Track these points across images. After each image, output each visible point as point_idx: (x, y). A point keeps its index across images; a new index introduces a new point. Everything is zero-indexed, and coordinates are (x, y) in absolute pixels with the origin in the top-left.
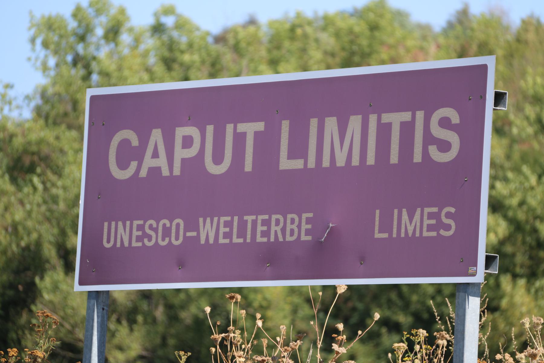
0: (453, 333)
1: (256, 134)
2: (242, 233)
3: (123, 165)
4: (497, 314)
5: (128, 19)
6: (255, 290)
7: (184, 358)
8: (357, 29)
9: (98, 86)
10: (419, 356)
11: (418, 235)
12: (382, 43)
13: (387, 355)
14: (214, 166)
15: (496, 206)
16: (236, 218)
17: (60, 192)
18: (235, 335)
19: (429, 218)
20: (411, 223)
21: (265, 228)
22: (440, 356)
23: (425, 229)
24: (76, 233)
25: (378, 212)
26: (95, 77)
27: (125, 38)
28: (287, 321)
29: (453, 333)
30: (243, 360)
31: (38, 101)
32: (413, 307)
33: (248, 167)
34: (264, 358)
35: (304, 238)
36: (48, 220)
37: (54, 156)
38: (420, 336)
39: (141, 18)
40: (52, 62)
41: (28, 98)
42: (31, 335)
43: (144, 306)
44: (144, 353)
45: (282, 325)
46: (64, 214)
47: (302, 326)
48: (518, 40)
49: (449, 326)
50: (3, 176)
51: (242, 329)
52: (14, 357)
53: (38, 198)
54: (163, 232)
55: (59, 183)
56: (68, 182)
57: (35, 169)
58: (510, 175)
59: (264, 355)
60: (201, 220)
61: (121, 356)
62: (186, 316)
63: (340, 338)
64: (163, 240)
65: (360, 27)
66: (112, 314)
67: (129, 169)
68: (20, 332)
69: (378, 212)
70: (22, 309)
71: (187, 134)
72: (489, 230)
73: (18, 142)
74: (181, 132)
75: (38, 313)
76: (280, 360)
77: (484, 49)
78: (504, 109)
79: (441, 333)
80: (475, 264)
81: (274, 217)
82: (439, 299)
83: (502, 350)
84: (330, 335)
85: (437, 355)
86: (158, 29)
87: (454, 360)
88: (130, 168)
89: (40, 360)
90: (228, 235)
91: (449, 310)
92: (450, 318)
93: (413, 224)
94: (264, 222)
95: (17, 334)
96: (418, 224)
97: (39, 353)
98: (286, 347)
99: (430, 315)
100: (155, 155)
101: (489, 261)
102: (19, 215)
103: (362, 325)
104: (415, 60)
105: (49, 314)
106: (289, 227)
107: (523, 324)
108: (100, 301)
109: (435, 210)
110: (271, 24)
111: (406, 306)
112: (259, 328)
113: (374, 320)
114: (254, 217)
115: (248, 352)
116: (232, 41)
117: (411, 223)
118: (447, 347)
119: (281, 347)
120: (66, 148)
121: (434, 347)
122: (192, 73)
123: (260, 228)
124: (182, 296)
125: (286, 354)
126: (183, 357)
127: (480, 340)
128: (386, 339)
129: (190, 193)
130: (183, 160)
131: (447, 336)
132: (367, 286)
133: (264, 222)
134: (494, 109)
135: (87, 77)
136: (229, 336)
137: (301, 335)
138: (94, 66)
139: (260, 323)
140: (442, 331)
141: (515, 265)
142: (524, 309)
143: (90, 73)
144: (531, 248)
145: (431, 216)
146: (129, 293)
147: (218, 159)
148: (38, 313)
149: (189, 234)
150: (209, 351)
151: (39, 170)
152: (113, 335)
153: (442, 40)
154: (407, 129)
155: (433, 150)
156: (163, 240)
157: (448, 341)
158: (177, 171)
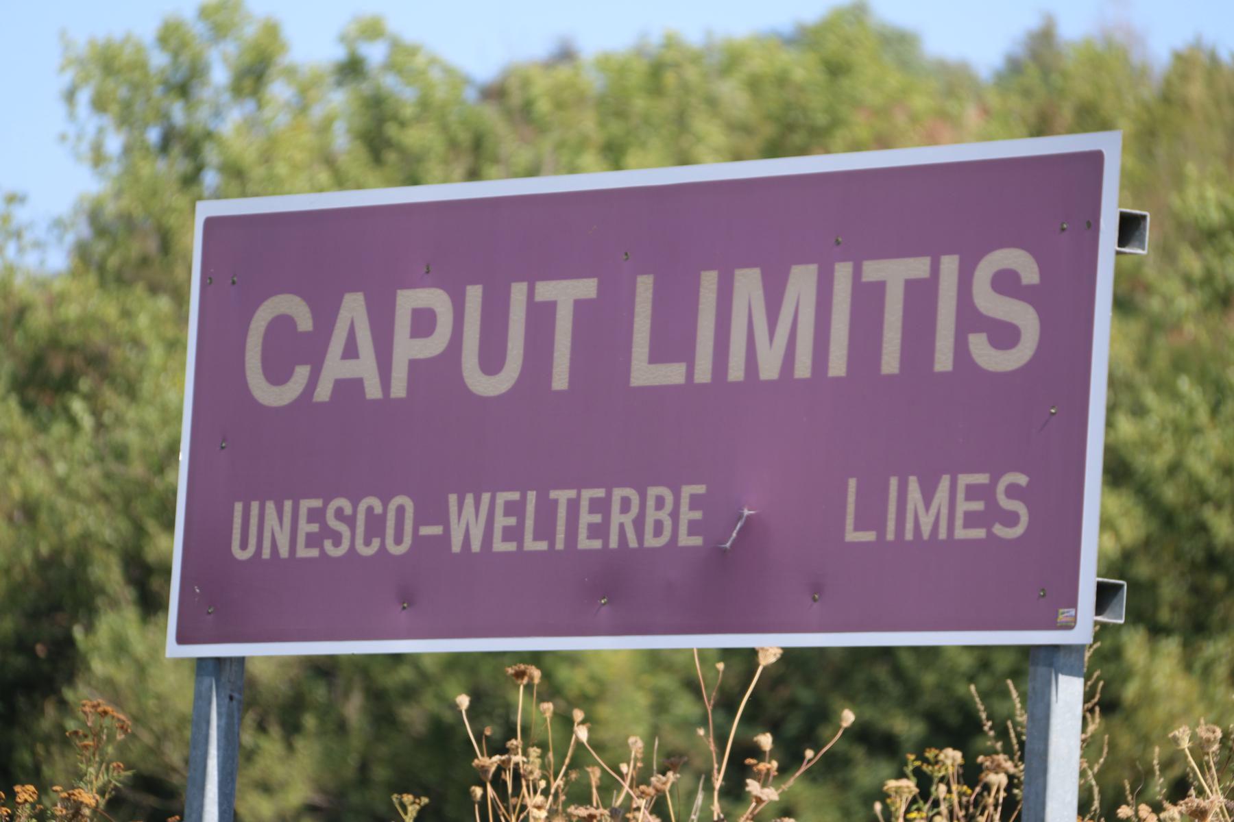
0: (1022, 759)
1: (579, 305)
2: (545, 529)
3: (277, 374)
4: (1116, 720)
5: (283, 48)
6: (572, 659)
7: (413, 810)
8: (799, 74)
9: (218, 195)
10: (943, 808)
11: (943, 534)
12: (857, 104)
13: (871, 807)
14: (485, 379)
15: (1118, 472)
16: (532, 496)
17: (132, 437)
18: (529, 761)
19: (969, 497)
20: (927, 506)
21: (597, 518)
22: (991, 809)
23: (959, 522)
24: (169, 526)
25: (852, 483)
26: (210, 178)
27: (279, 91)
28: (642, 729)
29: (1022, 759)
30: (543, 814)
31: (84, 230)
32: (928, 700)
33: (560, 380)
34: (592, 811)
35: (685, 540)
36: (105, 497)
37: (117, 354)
38: (944, 764)
39: (312, 46)
40: (114, 143)
41: (59, 225)
42: (63, 755)
43: (320, 692)
44: (317, 799)
45: (634, 735)
46: (145, 488)
47: (676, 740)
48: (1167, 98)
49: (1014, 741)
50: (4, 399)
51: (543, 746)
52: (27, 806)
53: (83, 446)
54: (369, 526)
55: (131, 414)
56: (151, 416)
57: (77, 382)
58: (1150, 398)
59: (591, 805)
60: (453, 499)
61: (264, 807)
62: (414, 716)
63: (763, 766)
64: (367, 543)
65: (803, 69)
66: (247, 710)
67: (290, 384)
68: (40, 749)
69: (852, 483)
70: (45, 696)
71: (421, 304)
72: (1101, 526)
73: (39, 319)
74: (408, 300)
75: (84, 705)
76: (629, 816)
77: (1090, 117)
78: (1139, 251)
79: (995, 757)
80: (1073, 602)
81: (618, 493)
82: (985, 681)
83: (1130, 798)
84: (741, 764)
85: (985, 808)
86: (352, 69)
87: (1024, 818)
88: (293, 379)
89: (87, 812)
90: (512, 534)
91: (1014, 706)
92: (1015, 725)
93: (932, 510)
94: (595, 505)
95: (34, 753)
96: (945, 512)
97: (84, 795)
98: (642, 787)
99: (965, 717)
100: (351, 351)
101: (1105, 595)
102: (39, 483)
103: (810, 737)
104: (932, 139)
105: (109, 709)
106: (651, 515)
107: (1176, 740)
108: (223, 680)
109: (982, 479)
110: (604, 63)
111: (910, 696)
112: (579, 744)
113: (840, 727)
114: (572, 493)
115: (556, 795)
116: (516, 99)
117: (927, 506)
118: (1008, 789)
119: (631, 787)
120: (148, 337)
121: (978, 789)
122: (434, 167)
123: (586, 518)
124: (405, 674)
125: (642, 803)
126: (410, 808)
127: (1083, 774)
128: (866, 773)
129: (429, 438)
130: (414, 365)
131: (1009, 765)
132: (821, 651)
133: (595, 505)
134: (1118, 253)
135: (191, 180)
136: (509, 760)
137: (672, 761)
138: (211, 155)
139: (582, 733)
140: (997, 753)
141: (1156, 606)
142: (1178, 705)
143: (199, 169)
144: (1194, 566)
145: (973, 492)
146: (285, 663)
147: (492, 361)
148: (84, 705)
149: (425, 531)
150: (469, 795)
151: (84, 384)
152: (250, 755)
153: (994, 100)
154: (921, 296)
155: (979, 346)
156: (367, 543)
157: (1011, 777)
158: (399, 389)
